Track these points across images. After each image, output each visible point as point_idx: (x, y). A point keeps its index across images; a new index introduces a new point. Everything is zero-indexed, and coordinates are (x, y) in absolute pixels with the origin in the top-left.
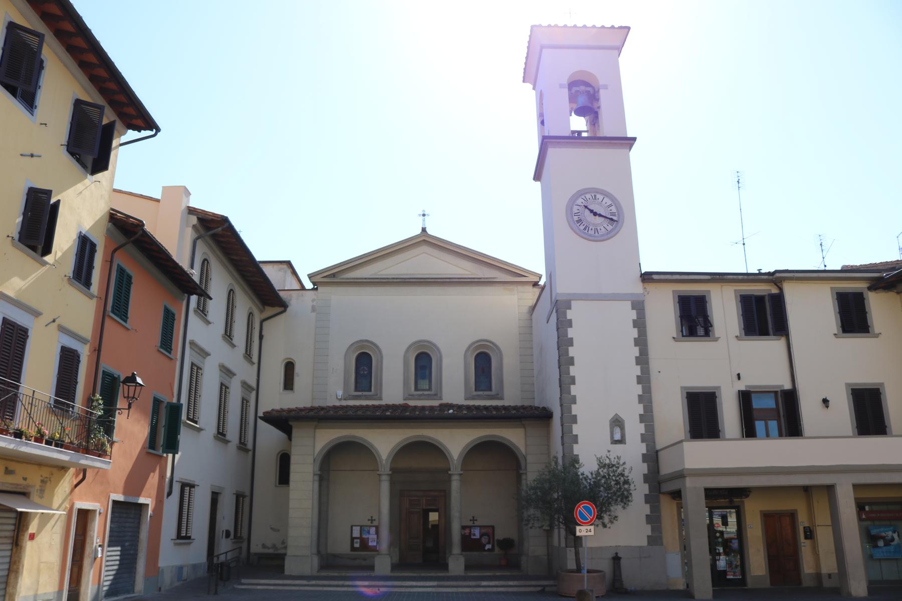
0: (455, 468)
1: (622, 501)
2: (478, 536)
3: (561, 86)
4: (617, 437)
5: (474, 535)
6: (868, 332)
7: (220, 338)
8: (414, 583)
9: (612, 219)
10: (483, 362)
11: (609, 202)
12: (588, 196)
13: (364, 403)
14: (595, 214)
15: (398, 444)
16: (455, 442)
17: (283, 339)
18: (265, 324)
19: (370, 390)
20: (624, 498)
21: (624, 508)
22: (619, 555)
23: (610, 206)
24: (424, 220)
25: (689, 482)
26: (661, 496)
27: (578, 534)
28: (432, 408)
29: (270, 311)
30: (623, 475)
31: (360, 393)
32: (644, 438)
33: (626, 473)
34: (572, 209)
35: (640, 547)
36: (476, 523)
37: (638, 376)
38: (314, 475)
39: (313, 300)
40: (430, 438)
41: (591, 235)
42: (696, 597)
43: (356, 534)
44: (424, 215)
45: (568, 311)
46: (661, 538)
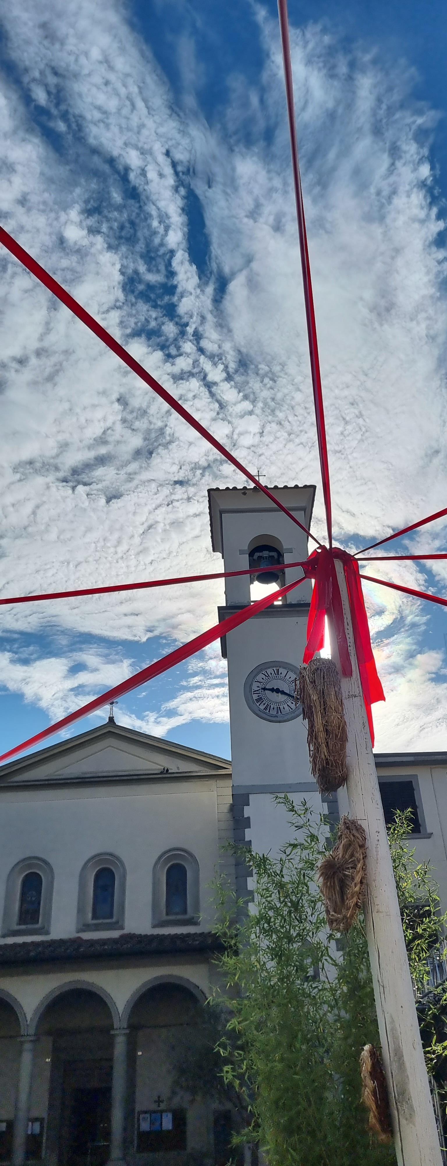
3: (242, 552)
12: (269, 671)
14: (278, 691)
16: (121, 988)
19: (111, 916)
28: (115, 941)
45: (245, 807)
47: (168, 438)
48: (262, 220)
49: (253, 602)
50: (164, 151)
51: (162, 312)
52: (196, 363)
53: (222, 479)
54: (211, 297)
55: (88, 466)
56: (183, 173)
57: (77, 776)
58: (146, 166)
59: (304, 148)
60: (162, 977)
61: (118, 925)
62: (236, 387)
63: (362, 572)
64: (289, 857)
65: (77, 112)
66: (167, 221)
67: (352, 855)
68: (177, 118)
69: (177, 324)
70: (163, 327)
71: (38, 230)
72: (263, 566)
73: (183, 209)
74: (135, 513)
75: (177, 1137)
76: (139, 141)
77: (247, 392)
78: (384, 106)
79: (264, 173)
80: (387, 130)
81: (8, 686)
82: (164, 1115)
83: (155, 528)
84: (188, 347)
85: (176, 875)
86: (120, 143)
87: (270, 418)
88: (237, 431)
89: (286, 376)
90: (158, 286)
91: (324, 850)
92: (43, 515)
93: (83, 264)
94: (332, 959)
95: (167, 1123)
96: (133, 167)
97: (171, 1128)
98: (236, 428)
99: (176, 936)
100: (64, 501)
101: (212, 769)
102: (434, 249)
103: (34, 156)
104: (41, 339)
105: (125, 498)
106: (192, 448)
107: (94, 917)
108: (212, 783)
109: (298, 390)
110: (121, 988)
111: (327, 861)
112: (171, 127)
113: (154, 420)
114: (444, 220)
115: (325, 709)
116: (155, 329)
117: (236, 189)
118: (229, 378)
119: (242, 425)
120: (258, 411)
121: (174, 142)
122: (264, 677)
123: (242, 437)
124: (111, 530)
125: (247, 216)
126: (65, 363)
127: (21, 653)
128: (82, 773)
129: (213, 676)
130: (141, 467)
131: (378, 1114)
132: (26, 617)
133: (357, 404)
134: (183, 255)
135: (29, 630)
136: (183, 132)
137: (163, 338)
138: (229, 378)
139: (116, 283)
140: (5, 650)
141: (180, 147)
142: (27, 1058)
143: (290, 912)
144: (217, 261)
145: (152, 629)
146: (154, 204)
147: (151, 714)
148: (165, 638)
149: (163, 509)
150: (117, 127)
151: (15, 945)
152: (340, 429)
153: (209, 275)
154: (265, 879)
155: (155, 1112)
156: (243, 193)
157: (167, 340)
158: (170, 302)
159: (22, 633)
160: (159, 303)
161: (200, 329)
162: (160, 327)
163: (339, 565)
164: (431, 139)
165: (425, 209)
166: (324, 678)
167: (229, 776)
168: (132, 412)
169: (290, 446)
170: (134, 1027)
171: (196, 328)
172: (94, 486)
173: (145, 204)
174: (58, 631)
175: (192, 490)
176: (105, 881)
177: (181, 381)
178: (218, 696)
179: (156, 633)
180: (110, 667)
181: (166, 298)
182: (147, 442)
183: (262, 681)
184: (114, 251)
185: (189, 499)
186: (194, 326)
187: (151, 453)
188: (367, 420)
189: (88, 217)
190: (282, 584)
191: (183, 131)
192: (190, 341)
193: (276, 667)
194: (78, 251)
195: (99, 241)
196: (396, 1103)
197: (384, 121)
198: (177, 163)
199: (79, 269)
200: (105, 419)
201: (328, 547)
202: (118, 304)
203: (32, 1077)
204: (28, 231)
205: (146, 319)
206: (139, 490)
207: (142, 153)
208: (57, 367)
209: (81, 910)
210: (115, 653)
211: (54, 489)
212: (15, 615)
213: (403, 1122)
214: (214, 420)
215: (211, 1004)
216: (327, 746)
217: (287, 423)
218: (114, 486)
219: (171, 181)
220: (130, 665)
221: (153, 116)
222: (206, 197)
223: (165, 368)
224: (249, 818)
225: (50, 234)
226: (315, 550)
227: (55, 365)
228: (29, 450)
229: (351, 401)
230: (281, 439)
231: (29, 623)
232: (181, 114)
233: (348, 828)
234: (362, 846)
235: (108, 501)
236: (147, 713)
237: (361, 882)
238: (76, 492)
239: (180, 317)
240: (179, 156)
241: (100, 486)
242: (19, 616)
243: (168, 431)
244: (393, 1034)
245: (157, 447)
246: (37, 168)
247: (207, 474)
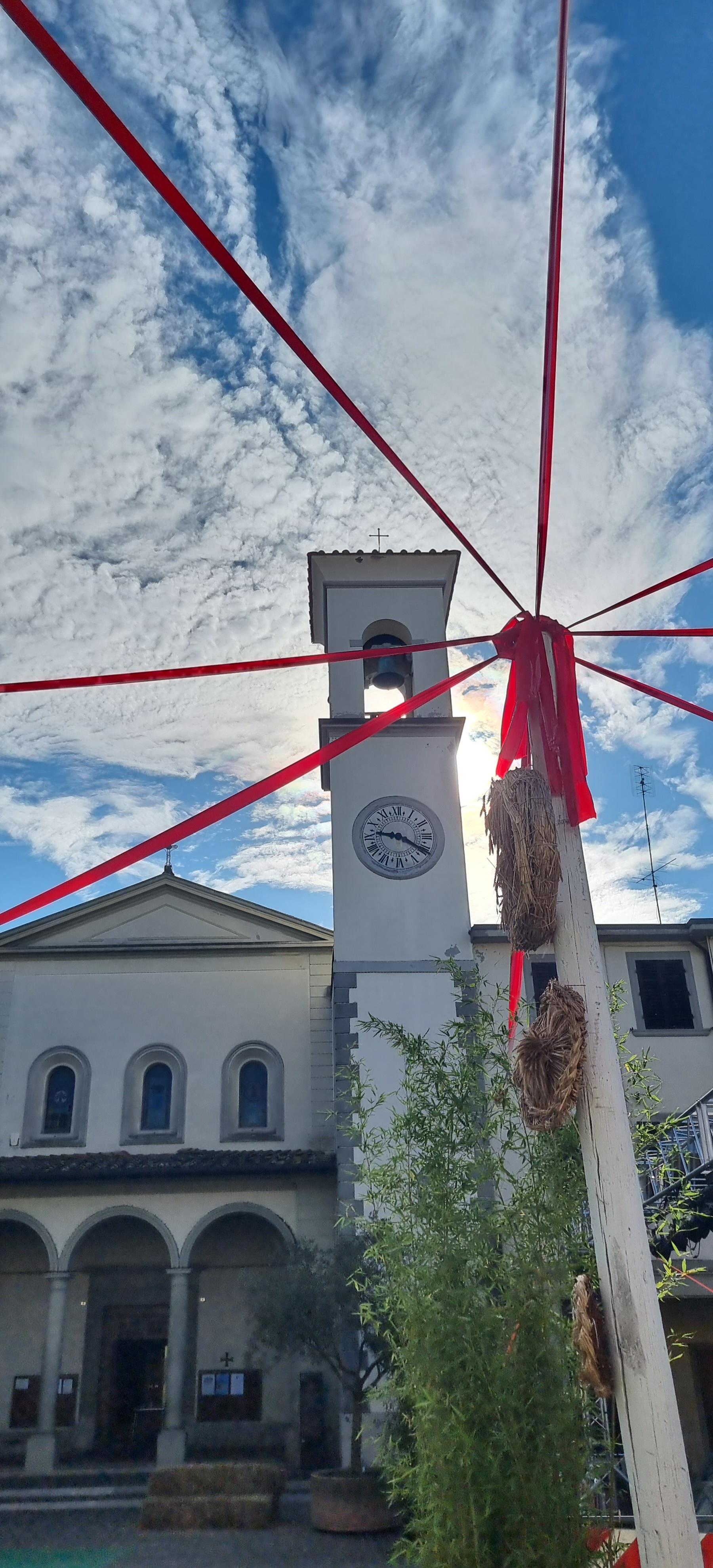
6: (691, 1026)
11: (421, 818)
12: (388, 809)
13: (57, 1151)
14: (398, 837)
15: (203, 1220)
16: (180, 1217)
19: (166, 1126)
31: (249, 1130)
47: (227, 502)
48: (358, 194)
49: (367, 714)
50: (222, 90)
51: (218, 325)
52: (266, 395)
53: (300, 561)
54: (287, 304)
55: (116, 538)
56: (249, 123)
57: (121, 942)
58: (197, 112)
59: (419, 89)
60: (234, 1205)
61: (175, 1138)
62: (320, 432)
63: (578, 654)
64: (452, 1041)
65: (100, 31)
66: (226, 193)
67: (566, 1031)
68: (242, 42)
69: (239, 342)
70: (220, 346)
71: (49, 202)
72: (383, 666)
73: (249, 177)
74: (180, 603)
75: (250, 1403)
76: (187, 74)
77: (334, 440)
78: (533, 31)
79: (361, 126)
80: (538, 66)
81: (9, 831)
82: (234, 1376)
83: (208, 625)
84: (255, 374)
85: (253, 1077)
86: (159, 77)
87: (367, 477)
88: (321, 494)
89: (389, 418)
90: (213, 286)
91: (501, 1033)
92: (53, 604)
93: (113, 253)
94: (508, 1174)
95: (237, 1387)
96: (179, 113)
97: (242, 1392)
98: (319, 489)
99: (253, 1154)
100: (83, 584)
101: (304, 940)
102: (601, 240)
103: (43, 92)
104: (52, 360)
105: (167, 581)
106: (260, 515)
107: (144, 1126)
108: (303, 958)
109: (407, 437)
111: (528, 1039)
112: (232, 55)
113: (208, 477)
114: (617, 198)
115: (531, 836)
116: (209, 349)
117: (323, 150)
118: (311, 419)
119: (328, 486)
120: (351, 466)
121: (235, 77)
122: (380, 817)
123: (328, 503)
124: (147, 627)
125: (336, 189)
126: (85, 394)
127: (26, 788)
128: (129, 939)
129: (285, 827)
130: (189, 541)
131: (598, 1359)
132: (32, 740)
133: (489, 460)
134: (249, 243)
135: (37, 759)
136: (251, 64)
137: (219, 361)
138: (311, 419)
139: (156, 282)
140: (4, 783)
141: (245, 84)
142: (57, 1300)
143: (451, 1112)
144: (296, 253)
145: (204, 761)
146: (208, 167)
147: (202, 874)
148: (221, 774)
149: (219, 600)
150: (156, 54)
151: (39, 1159)
152: (467, 494)
153: (283, 272)
154: (420, 1068)
155: (223, 1372)
156: (332, 155)
157: (226, 364)
158: (230, 310)
159: (26, 762)
160: (214, 311)
161: (272, 349)
162: (216, 346)
163: (547, 640)
164: (601, 81)
165: (590, 180)
166: (530, 794)
167: (330, 949)
168: (177, 463)
169: (396, 516)
170: (196, 1267)
171: (266, 348)
172: (124, 565)
173: (196, 167)
174: (76, 760)
175: (258, 574)
176: (158, 1082)
177: (245, 422)
178: (292, 854)
179: (209, 767)
180: (148, 811)
181: (225, 304)
182: (197, 507)
183: (377, 822)
184: (155, 235)
185: (255, 587)
186: (263, 346)
187: (203, 522)
188: (502, 482)
189: (116, 185)
190: (408, 694)
191: (250, 62)
192: (258, 367)
193: (397, 804)
194: (104, 234)
195: (133, 219)
196: (620, 1349)
197: (533, 51)
198: (241, 108)
199: (106, 258)
200: (140, 473)
201: (533, 614)
202: (160, 311)
203: (65, 1322)
204: (33, 204)
205: (195, 334)
206: (184, 572)
207: (191, 92)
208: (75, 399)
209: (126, 1117)
210: (154, 792)
211: (68, 568)
212: (17, 738)
213: (629, 1371)
214: (291, 477)
215: (342, 1226)
216: (533, 886)
217: (389, 485)
218: (152, 565)
219: (231, 134)
220: (175, 809)
221: (206, 39)
222: (281, 160)
223: (223, 402)
224: (355, 1004)
225: (67, 209)
226: (514, 619)
227: (72, 396)
228: (36, 514)
229: (482, 455)
230: (382, 507)
231: (37, 749)
232: (247, 37)
233: (559, 996)
234: (580, 1020)
235: (143, 586)
236: (195, 872)
237: (579, 1067)
238: (99, 571)
239: (244, 333)
240: (243, 97)
241: (132, 565)
242: (22, 739)
243: (227, 492)
244: (617, 1262)
245: (211, 514)
246: (45, 110)
247: (279, 552)
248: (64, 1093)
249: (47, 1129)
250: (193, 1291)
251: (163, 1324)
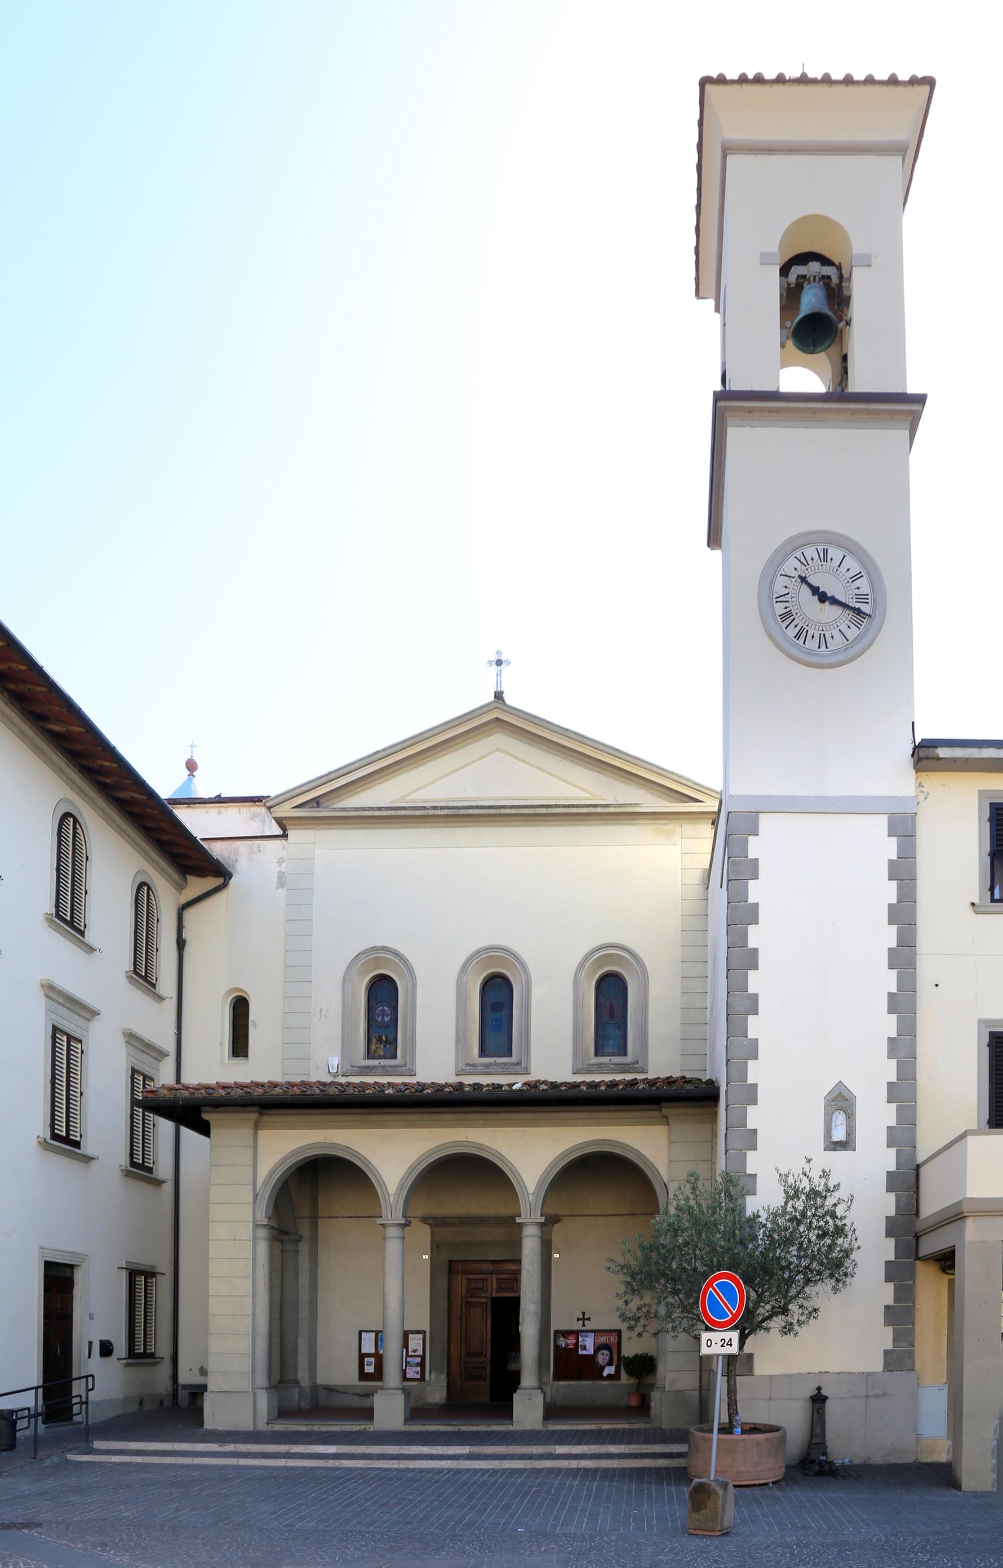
0: (530, 1213)
1: (832, 1276)
2: (590, 1350)
4: (839, 1134)
5: (584, 1348)
7: (41, 921)
8: (425, 1450)
9: (858, 612)
10: (611, 995)
12: (810, 552)
14: (823, 598)
16: (531, 1154)
17: (228, 944)
18: (188, 914)
20: (835, 1267)
21: (835, 1290)
22: (824, 1392)
23: (858, 576)
24: (499, 675)
25: (972, 1231)
26: (918, 1263)
27: (705, 1350)
29: (197, 886)
30: (833, 1215)
31: (605, 1060)
32: (893, 1138)
33: (840, 1211)
34: (772, 584)
35: (869, 1374)
36: (589, 1325)
37: (890, 995)
38: (256, 1226)
39: (281, 861)
40: (480, 1147)
41: (810, 653)
42: (964, 1488)
43: (368, 1347)
44: (499, 663)
46: (911, 1355)
107: (483, 1053)
110: (531, 1154)
122: (798, 565)
142: (393, 1248)
170: (550, 1221)
176: (497, 997)
209: (461, 1040)
248: (386, 1009)
249: (369, 1054)
250: (546, 1247)
251: (515, 1278)
